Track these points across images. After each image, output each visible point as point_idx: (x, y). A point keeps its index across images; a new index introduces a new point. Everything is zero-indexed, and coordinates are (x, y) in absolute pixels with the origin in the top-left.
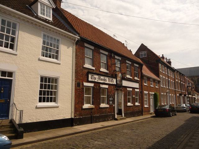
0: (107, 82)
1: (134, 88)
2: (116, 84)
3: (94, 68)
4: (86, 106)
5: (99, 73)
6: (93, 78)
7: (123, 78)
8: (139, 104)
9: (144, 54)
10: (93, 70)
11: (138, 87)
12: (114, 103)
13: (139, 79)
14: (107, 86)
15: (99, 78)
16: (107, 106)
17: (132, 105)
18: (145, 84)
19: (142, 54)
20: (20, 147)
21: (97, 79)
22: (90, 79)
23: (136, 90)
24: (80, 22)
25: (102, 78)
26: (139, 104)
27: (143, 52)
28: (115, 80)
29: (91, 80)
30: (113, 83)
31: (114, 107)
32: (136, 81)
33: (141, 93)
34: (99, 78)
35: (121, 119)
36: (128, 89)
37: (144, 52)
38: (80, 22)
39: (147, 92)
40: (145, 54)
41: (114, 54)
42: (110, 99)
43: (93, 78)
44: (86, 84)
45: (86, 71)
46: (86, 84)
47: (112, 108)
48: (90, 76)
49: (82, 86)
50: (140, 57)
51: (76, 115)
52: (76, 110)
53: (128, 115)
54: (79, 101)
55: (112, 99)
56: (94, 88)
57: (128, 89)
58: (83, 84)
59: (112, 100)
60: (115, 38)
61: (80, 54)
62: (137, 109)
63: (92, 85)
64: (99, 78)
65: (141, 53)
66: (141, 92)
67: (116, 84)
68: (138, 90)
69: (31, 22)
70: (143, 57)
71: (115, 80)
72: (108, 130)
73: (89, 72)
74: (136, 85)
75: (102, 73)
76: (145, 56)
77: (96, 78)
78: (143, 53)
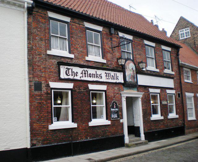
0: (104, 79)
1: (163, 89)
2: (123, 82)
3: (72, 56)
4: (154, 117)
5: (85, 64)
6: (70, 73)
7: (139, 71)
8: (177, 116)
9: (186, 33)
10: (71, 59)
11: (173, 87)
12: (120, 116)
13: (173, 73)
14: (104, 87)
15: (85, 74)
16: (108, 122)
17: (162, 118)
18: (186, 81)
19: (183, 34)
20: (115, 160)
21: (79, 75)
22: (63, 76)
23: (168, 91)
24: (111, 6)
25: (112, 73)
26: (177, 116)
27: (184, 30)
28: (122, 75)
29: (66, 77)
30: (118, 81)
31: (122, 124)
32: (168, 76)
33: (179, 96)
34: (85, 74)
35: (137, 145)
36: (91, 87)
37: (186, 30)
38: (111, 6)
39: (192, 95)
40: (188, 32)
41: (115, 29)
42: (112, 110)
43: (70, 73)
44: (53, 85)
45: (55, 62)
46: (53, 85)
47: (116, 124)
48: (63, 69)
49: (47, 89)
50: (181, 39)
51: (35, 142)
52: (34, 133)
53: (150, 137)
54: (40, 118)
55: (116, 110)
56: (75, 91)
57: (151, 90)
58: (48, 86)
59: (117, 112)
60: (132, 10)
61: (38, 31)
62: (173, 125)
63: (70, 86)
64: (107, 75)
65: (181, 32)
66: (179, 94)
67: (123, 82)
68: (173, 92)
69: (12, 3)
70: (185, 37)
71: (120, 76)
72: (162, 151)
73: (62, 62)
74: (169, 83)
75: (90, 64)
76: (181, 34)
77: (79, 73)
78: (184, 32)
